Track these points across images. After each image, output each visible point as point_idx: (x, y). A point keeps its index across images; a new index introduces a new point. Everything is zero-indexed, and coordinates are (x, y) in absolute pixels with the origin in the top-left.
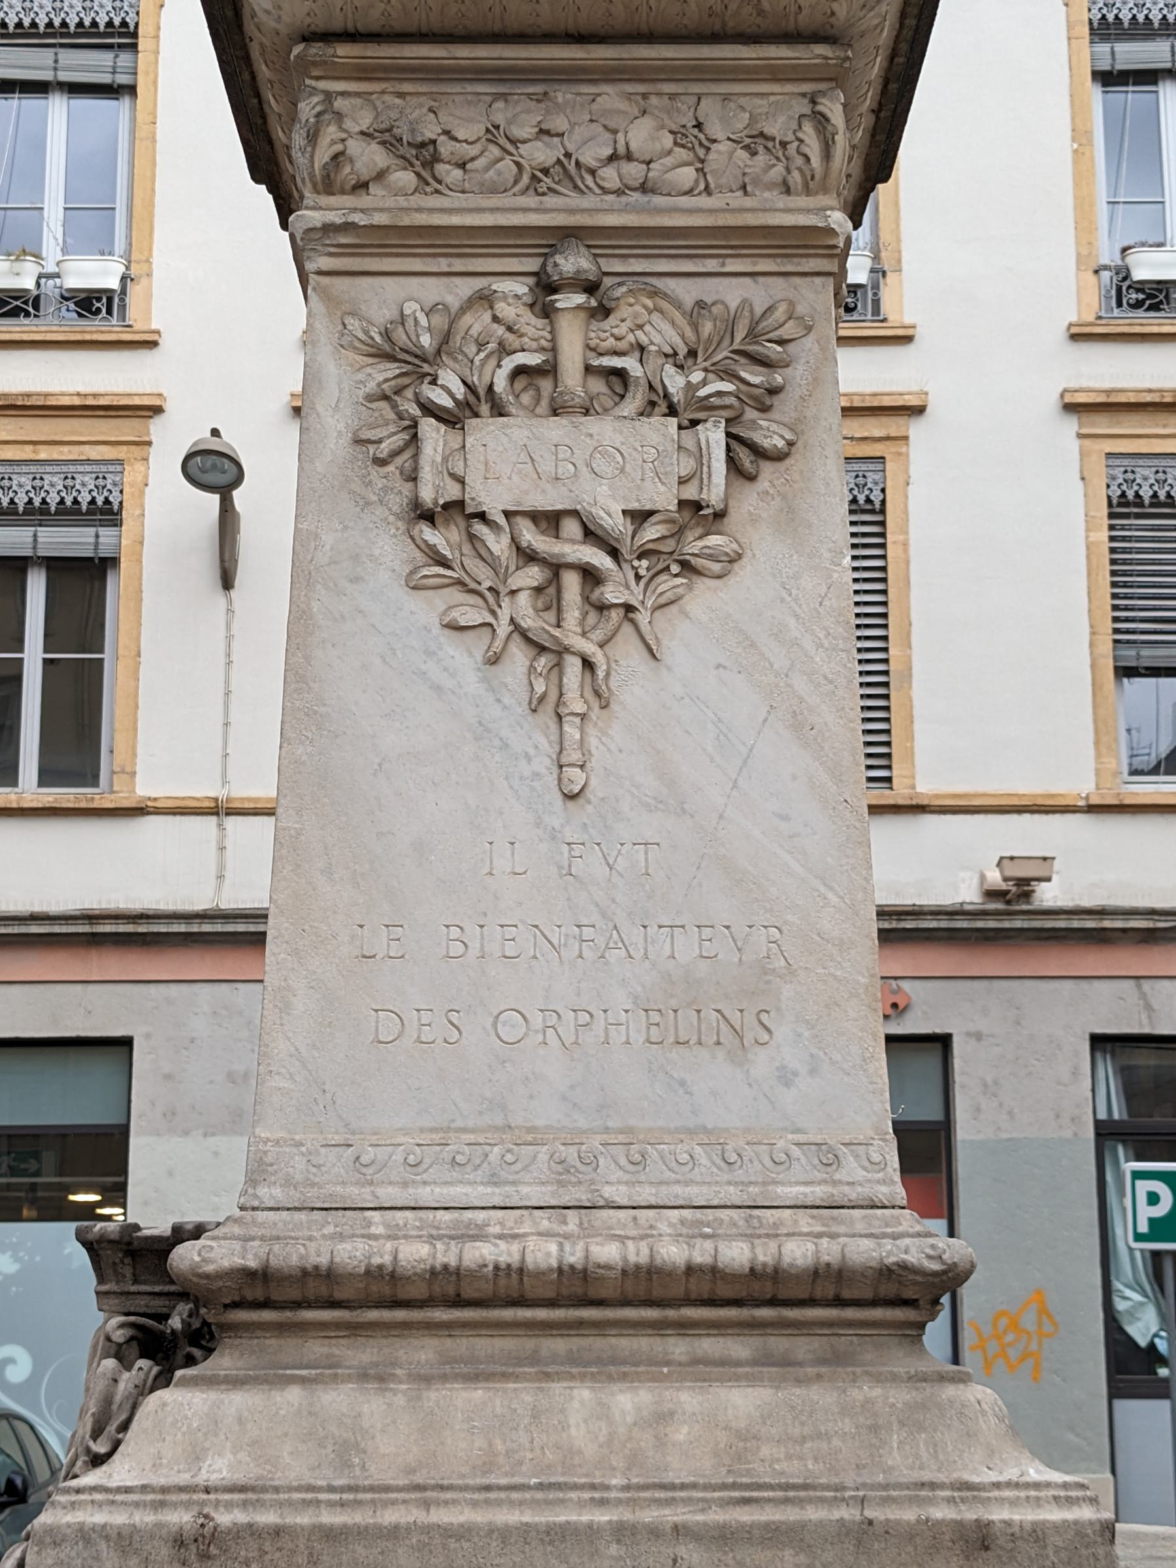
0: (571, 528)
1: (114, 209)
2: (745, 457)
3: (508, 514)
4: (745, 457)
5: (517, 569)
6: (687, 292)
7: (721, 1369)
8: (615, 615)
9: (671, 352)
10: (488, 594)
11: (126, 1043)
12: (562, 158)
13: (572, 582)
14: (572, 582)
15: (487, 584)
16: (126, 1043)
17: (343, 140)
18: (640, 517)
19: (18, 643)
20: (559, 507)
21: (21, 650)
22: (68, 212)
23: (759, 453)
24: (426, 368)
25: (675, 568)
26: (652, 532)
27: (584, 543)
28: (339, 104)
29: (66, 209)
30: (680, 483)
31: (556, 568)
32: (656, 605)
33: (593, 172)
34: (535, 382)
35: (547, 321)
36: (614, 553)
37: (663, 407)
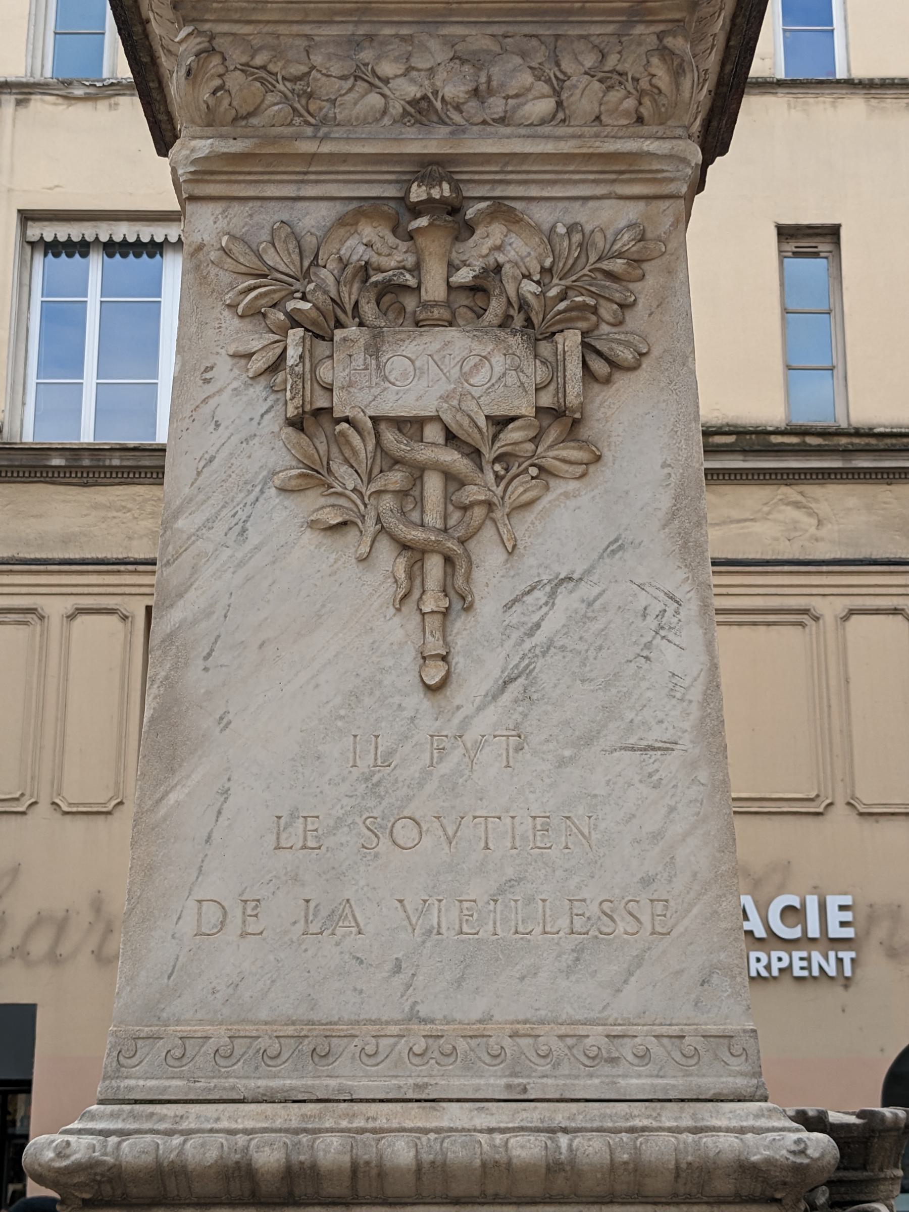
0: (433, 433)
1: (103, 34)
2: (599, 366)
3: (375, 420)
4: (599, 366)
5: (381, 472)
6: (542, 215)
7: (745, 1124)
8: (478, 513)
9: (527, 273)
10: (354, 496)
11: (832, 233)
12: (430, 95)
13: (433, 485)
14: (433, 485)
15: (351, 486)
16: (832, 233)
17: (220, 76)
18: (501, 423)
19: (79, 371)
20: (423, 413)
21: (82, 378)
22: (58, 36)
23: (613, 364)
24: (297, 285)
25: (534, 471)
26: (512, 434)
27: (446, 445)
28: (218, 43)
29: (56, 33)
30: (537, 390)
31: (418, 472)
32: (517, 504)
33: (458, 108)
34: (401, 300)
35: (410, 243)
36: (475, 454)
37: (518, 321)
